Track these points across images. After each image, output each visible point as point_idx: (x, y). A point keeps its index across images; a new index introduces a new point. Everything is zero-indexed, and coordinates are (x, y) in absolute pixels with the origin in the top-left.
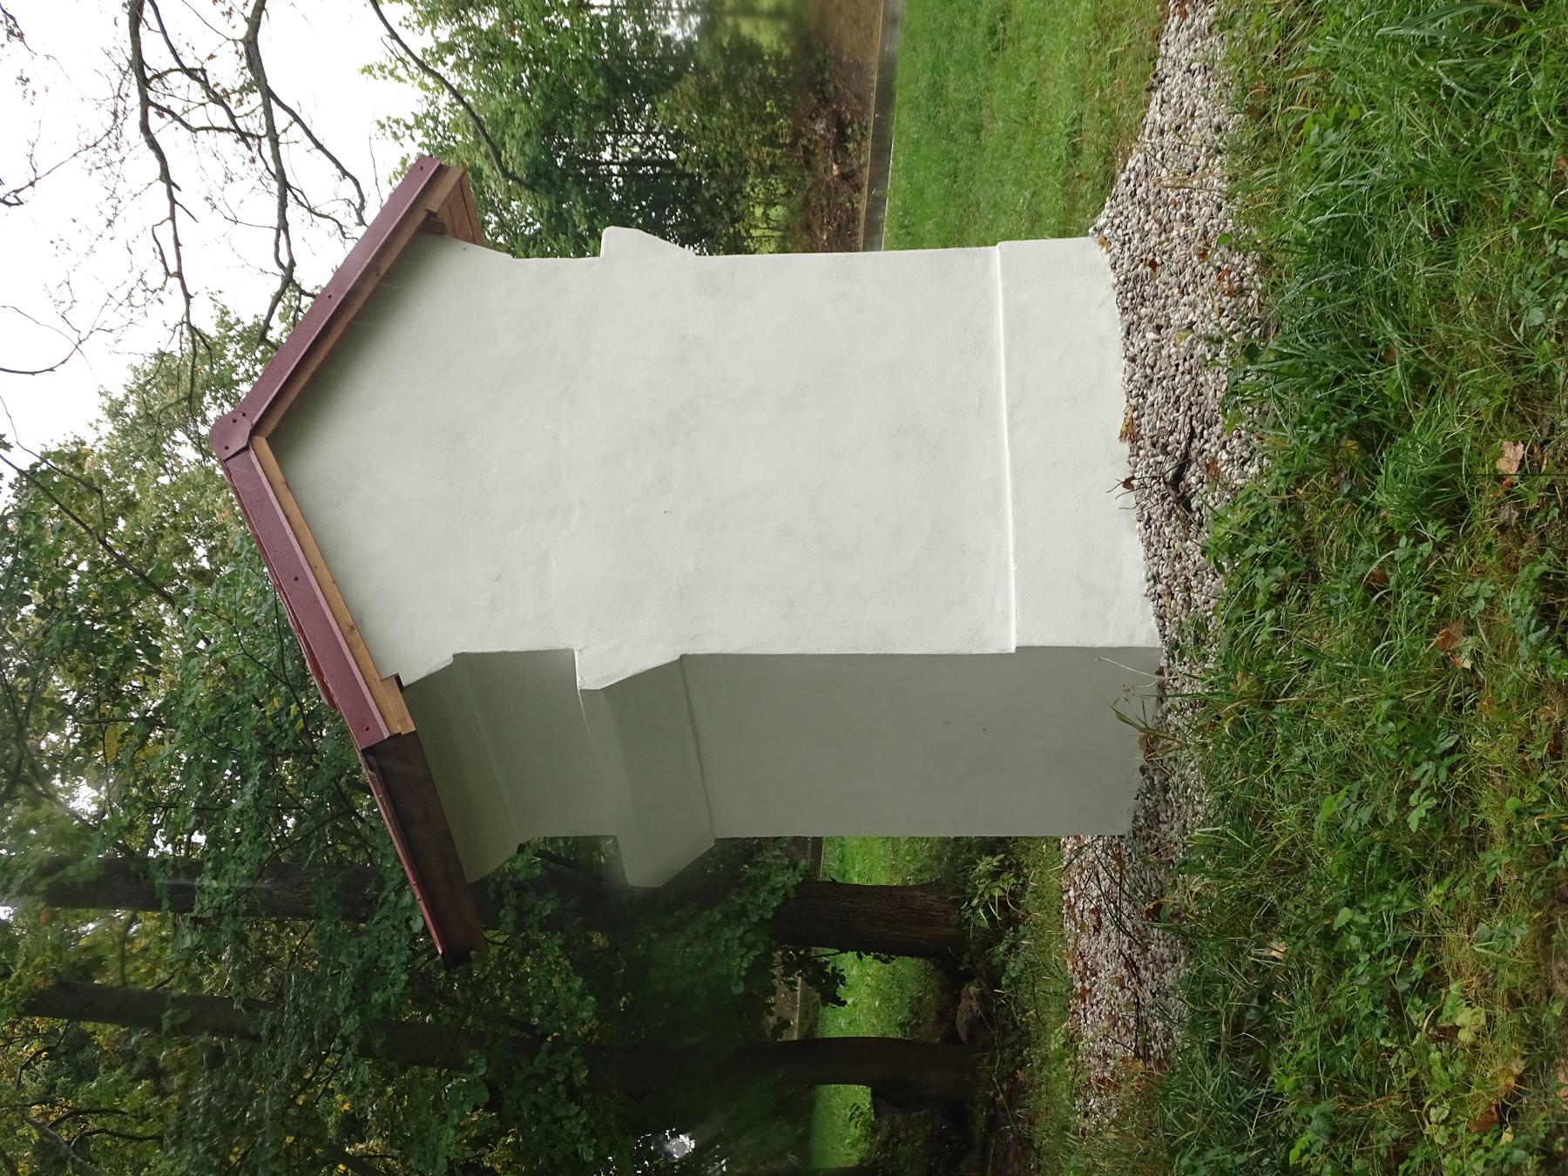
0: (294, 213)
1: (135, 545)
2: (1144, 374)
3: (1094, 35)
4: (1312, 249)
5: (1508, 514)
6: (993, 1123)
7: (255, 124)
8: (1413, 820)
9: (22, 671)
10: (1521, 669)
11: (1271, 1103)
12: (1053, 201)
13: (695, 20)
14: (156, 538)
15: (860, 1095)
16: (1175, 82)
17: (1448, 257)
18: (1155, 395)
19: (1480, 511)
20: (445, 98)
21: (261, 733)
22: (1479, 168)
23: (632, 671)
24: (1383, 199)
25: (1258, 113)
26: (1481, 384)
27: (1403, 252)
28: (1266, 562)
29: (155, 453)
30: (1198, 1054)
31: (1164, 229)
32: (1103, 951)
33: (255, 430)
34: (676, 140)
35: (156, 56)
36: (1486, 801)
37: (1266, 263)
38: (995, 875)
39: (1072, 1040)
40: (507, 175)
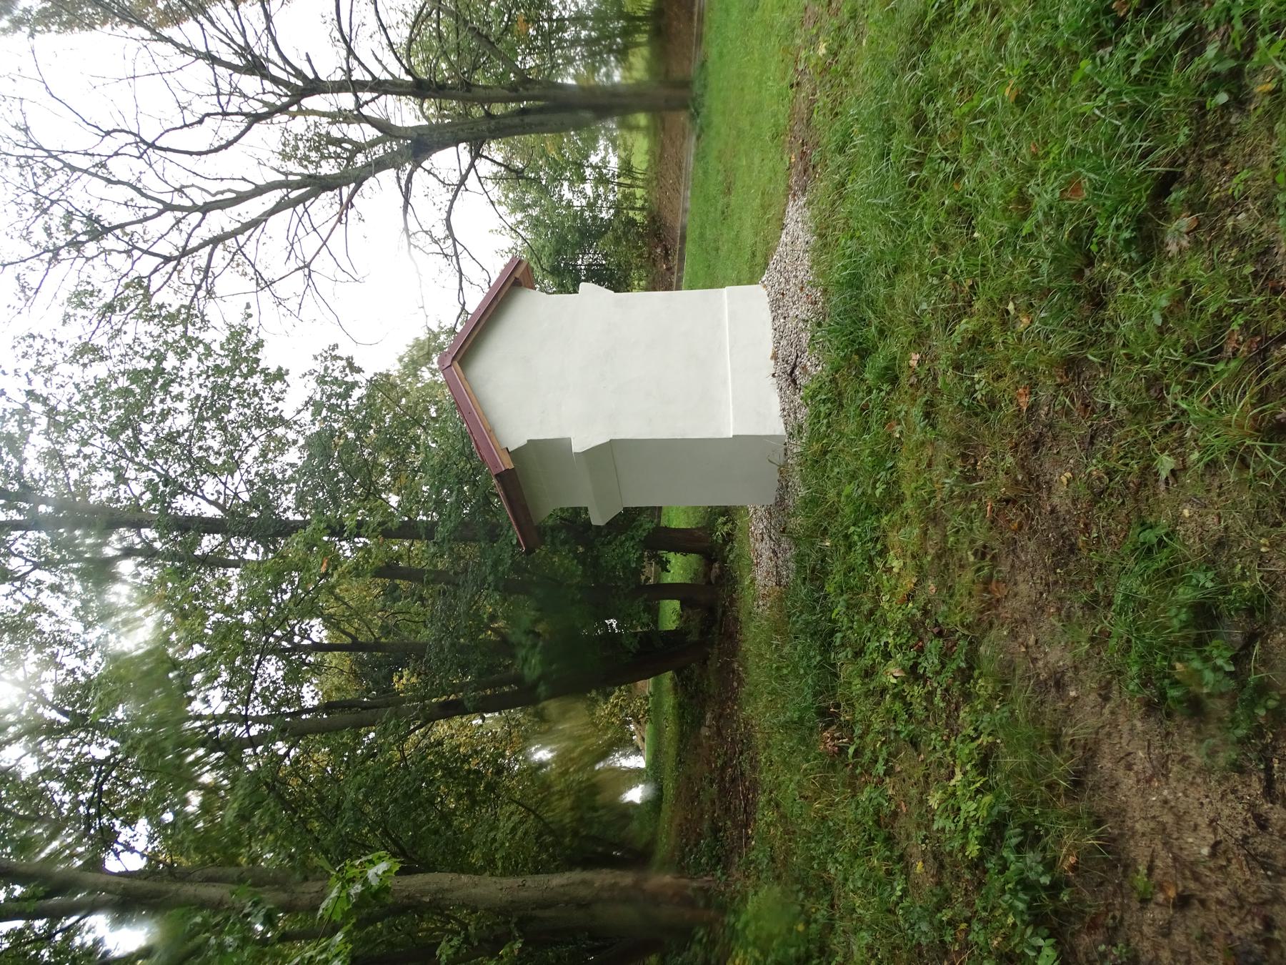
0: (465, 284)
1: (409, 408)
2: (780, 334)
3: (761, 212)
4: (842, 284)
5: (913, 380)
6: (724, 613)
7: (450, 251)
8: (878, 492)
9: (370, 454)
10: (917, 436)
11: (825, 598)
12: (745, 275)
13: (612, 211)
14: (417, 404)
15: (676, 604)
16: (791, 226)
17: (892, 285)
18: (784, 342)
19: (903, 380)
20: (520, 241)
21: (457, 476)
22: (903, 252)
23: (593, 445)
24: (868, 265)
25: (822, 236)
26: (904, 333)
27: (876, 288)
28: (824, 401)
29: (415, 375)
30: (799, 581)
31: (787, 281)
32: (764, 548)
33: (454, 359)
34: (605, 256)
35: (413, 227)
36: (904, 484)
37: (825, 291)
38: (725, 524)
39: (753, 580)
40: (543, 270)
